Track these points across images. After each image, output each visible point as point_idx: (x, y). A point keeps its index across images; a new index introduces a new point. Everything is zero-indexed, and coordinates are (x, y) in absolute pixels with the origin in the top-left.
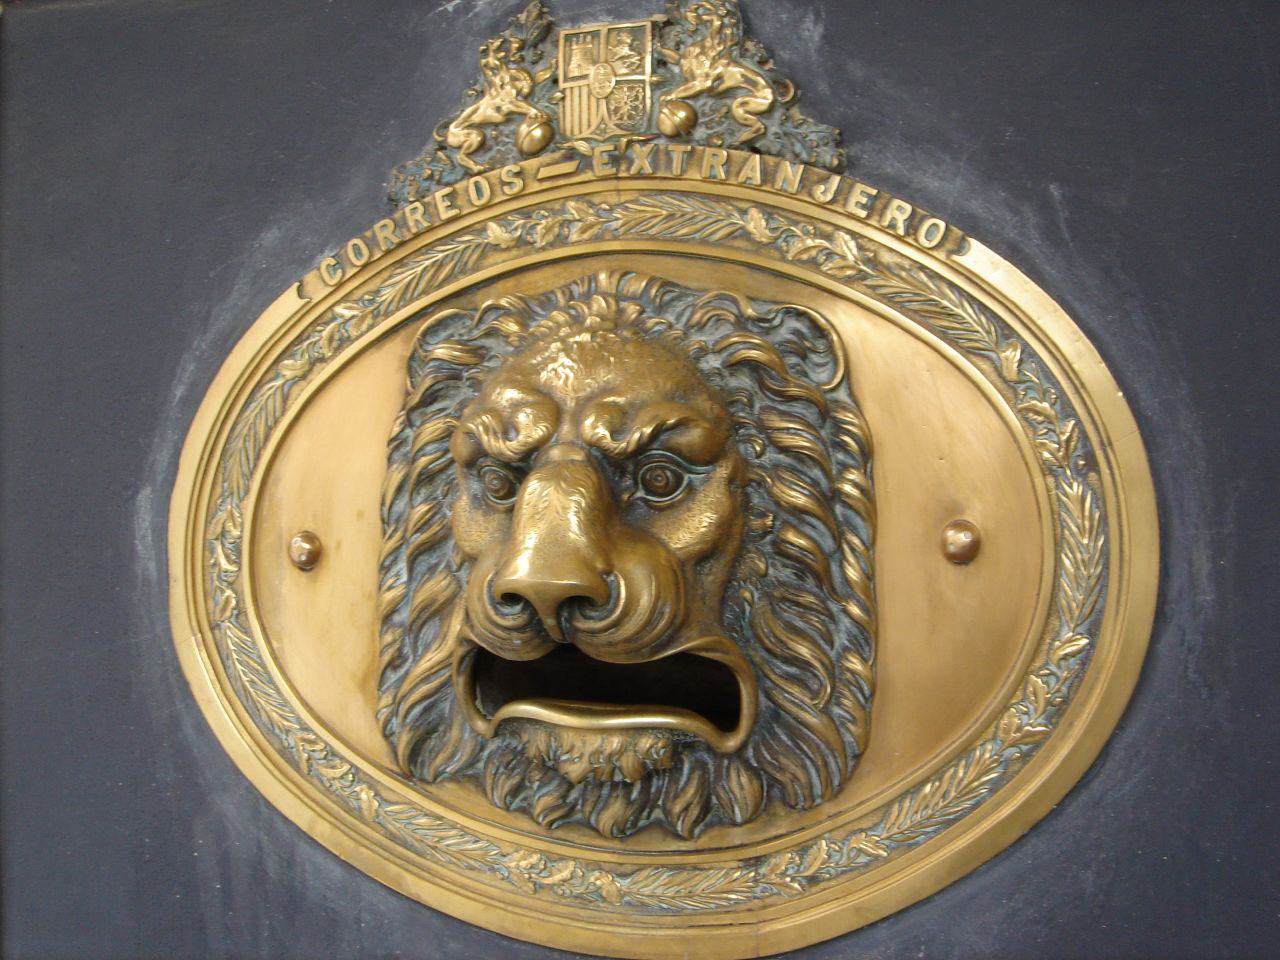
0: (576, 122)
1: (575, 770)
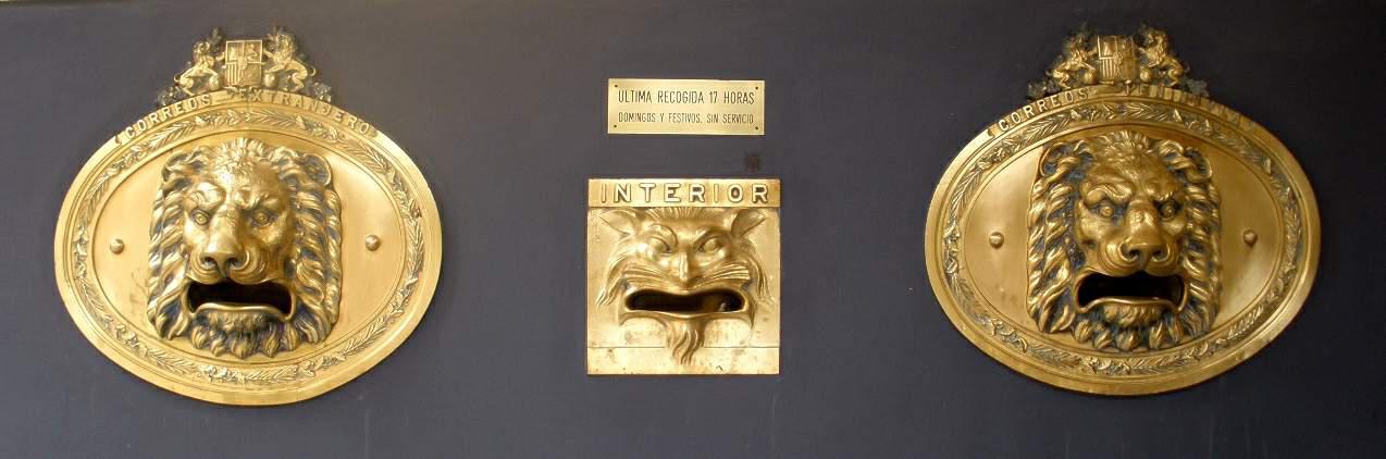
1: (228, 327)
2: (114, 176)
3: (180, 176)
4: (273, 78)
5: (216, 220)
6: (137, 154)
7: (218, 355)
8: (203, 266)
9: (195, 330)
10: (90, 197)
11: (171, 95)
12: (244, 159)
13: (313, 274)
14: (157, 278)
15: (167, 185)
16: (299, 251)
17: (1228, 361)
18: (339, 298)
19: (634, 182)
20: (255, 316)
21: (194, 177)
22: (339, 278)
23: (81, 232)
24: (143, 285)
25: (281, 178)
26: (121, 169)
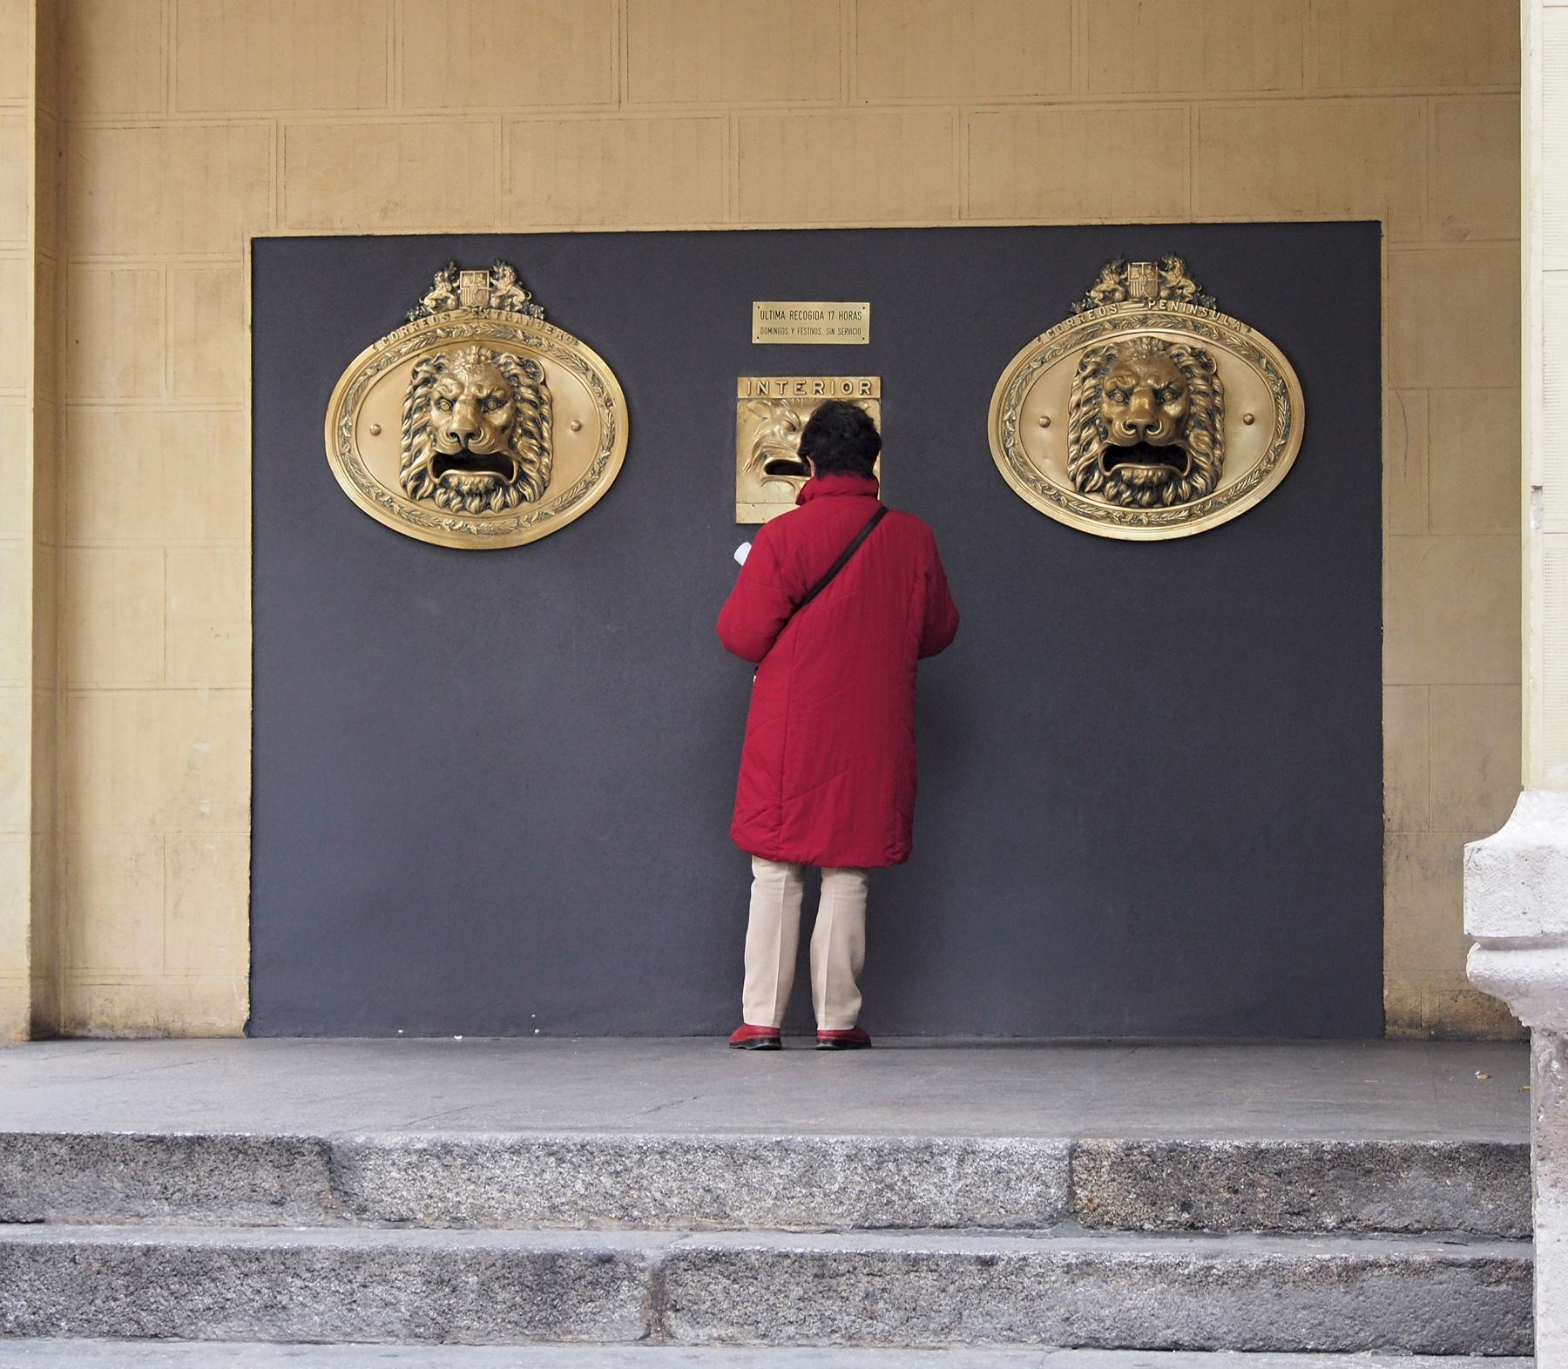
5: (457, 406)
13: (531, 449)
15: (415, 382)
19: (808, 379)
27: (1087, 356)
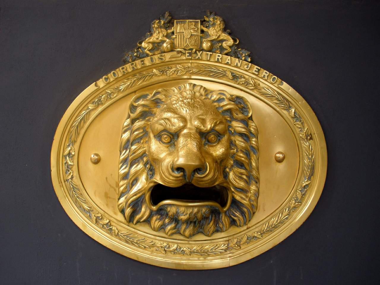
0: (180, 43)
2: (93, 110)
3: (145, 109)
4: (209, 44)
5: (181, 140)
6: (110, 94)
7: (169, 236)
8: (173, 174)
9: (154, 218)
10: (76, 124)
11: (135, 54)
12: (193, 97)
13: (241, 178)
14: (126, 181)
16: (232, 162)
17: (179, 264)
18: (257, 194)
20: (204, 210)
21: (155, 110)
22: (257, 181)
23: (69, 148)
24: (115, 186)
25: (220, 111)
26: (99, 104)
27: (138, 99)
